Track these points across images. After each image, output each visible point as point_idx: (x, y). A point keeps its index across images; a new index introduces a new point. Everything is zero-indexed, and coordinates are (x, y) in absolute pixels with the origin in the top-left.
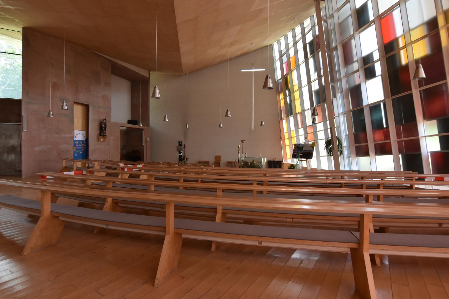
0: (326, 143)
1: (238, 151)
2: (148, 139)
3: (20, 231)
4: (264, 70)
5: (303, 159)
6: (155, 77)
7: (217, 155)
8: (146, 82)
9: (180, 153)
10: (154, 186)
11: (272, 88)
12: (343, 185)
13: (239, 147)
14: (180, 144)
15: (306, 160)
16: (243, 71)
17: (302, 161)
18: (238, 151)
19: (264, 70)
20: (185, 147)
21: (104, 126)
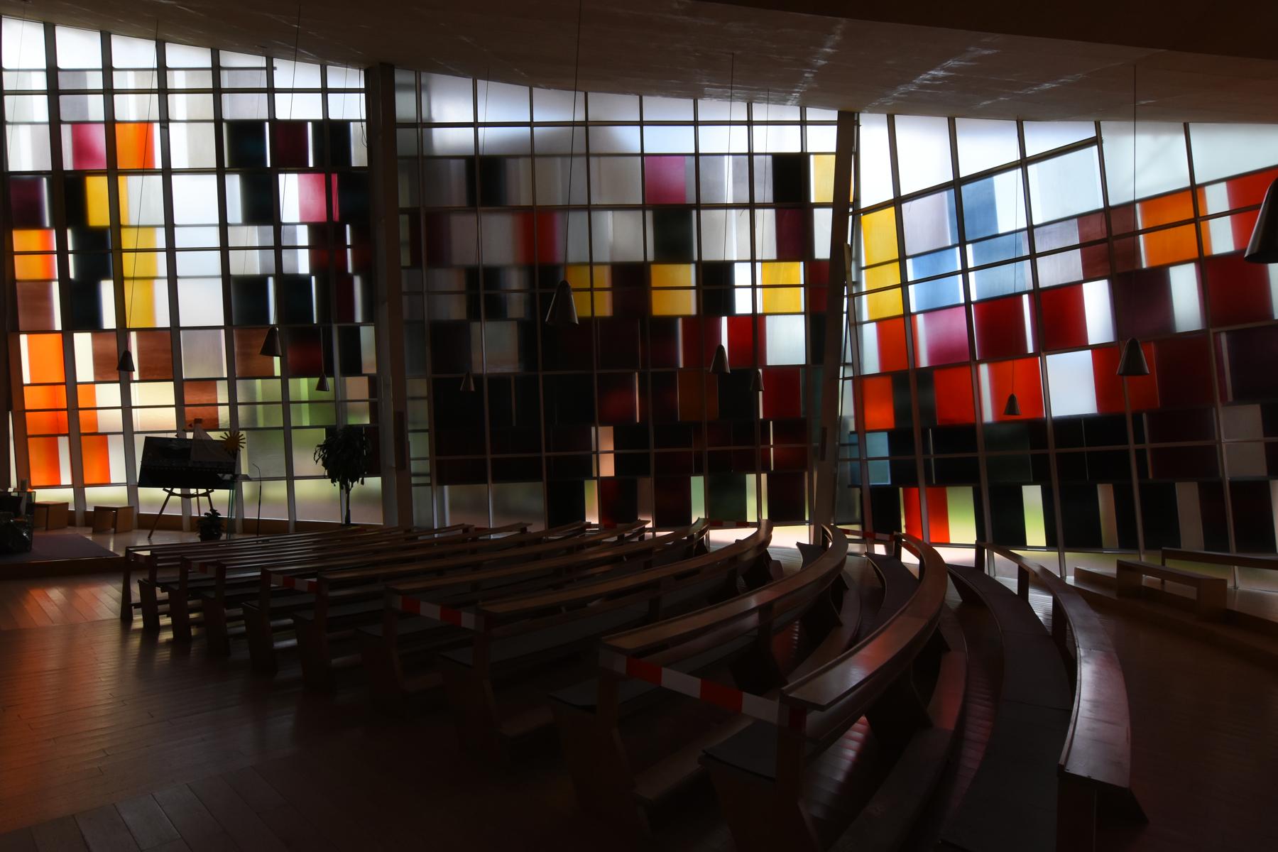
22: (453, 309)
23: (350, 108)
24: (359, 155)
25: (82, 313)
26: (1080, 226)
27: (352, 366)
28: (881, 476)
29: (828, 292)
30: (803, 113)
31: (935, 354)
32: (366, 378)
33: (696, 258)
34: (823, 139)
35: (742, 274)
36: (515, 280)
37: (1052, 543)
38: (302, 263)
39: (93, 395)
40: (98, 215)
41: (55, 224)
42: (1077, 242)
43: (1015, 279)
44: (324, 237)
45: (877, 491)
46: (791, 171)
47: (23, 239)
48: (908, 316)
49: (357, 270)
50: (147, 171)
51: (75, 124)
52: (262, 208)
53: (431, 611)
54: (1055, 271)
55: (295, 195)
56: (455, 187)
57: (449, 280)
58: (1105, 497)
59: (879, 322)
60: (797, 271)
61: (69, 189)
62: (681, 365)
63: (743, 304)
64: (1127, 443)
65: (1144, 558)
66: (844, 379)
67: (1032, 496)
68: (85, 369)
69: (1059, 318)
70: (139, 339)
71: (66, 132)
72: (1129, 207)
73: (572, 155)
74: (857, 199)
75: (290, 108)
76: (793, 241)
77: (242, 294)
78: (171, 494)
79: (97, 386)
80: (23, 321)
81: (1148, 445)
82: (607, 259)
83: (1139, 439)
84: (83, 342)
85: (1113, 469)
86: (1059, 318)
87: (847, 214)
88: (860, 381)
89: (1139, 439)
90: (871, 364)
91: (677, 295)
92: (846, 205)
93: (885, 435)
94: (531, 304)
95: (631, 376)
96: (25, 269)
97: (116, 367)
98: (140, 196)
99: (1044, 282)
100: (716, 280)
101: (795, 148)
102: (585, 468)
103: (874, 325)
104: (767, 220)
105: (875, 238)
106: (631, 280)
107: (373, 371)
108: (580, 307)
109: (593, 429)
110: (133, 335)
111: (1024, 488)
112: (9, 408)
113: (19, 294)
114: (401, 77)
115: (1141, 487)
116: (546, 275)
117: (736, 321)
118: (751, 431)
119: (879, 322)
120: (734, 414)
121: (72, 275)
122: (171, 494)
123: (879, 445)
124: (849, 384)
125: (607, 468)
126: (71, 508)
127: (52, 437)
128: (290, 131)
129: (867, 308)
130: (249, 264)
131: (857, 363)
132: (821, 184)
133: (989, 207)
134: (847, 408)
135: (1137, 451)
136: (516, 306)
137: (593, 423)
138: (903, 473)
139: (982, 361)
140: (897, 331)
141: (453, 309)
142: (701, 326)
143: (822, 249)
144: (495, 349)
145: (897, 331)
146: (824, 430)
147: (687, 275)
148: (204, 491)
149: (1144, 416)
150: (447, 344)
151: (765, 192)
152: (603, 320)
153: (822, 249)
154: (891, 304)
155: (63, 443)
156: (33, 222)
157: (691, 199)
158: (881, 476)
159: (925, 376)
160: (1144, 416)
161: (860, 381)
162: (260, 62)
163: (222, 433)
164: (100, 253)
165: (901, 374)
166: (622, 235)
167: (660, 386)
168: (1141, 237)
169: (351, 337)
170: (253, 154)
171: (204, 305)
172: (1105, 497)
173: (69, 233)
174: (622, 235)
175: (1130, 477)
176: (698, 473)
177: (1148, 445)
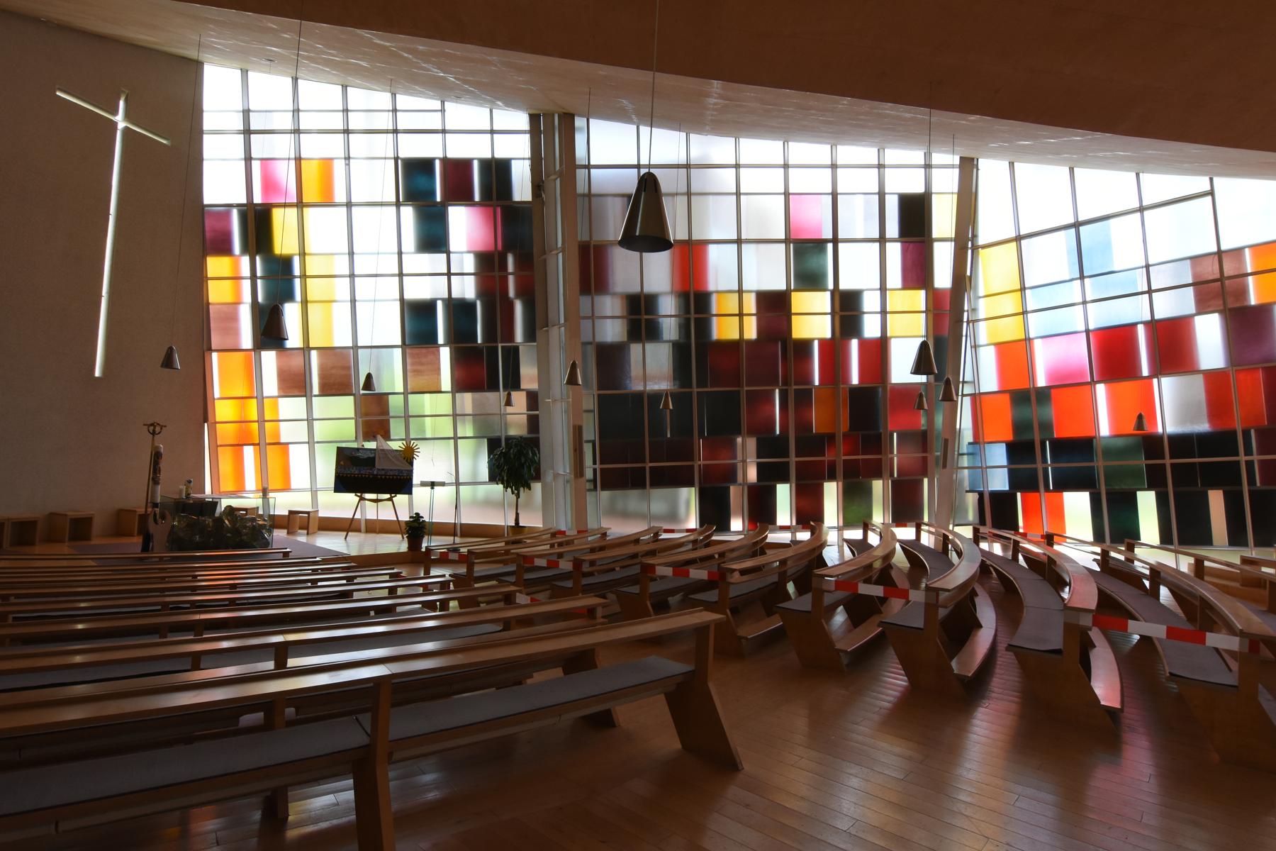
15: (390, 499)
22: (612, 331)
23: (516, 149)
24: (522, 189)
25: (269, 331)
26: (1193, 267)
27: (513, 382)
28: (999, 481)
29: (948, 319)
30: (928, 155)
31: (1051, 375)
32: (524, 393)
33: (831, 286)
34: (945, 185)
35: (870, 302)
36: (668, 306)
37: (1166, 539)
38: (466, 289)
39: (276, 408)
40: (284, 243)
41: (246, 249)
42: (1190, 281)
43: (1133, 312)
44: (488, 264)
45: (996, 496)
46: (915, 213)
47: (216, 265)
48: (1028, 341)
49: (518, 295)
50: (329, 203)
51: (263, 160)
52: (433, 238)
53: (453, 604)
54: (1168, 306)
55: (465, 226)
56: (614, 224)
57: (610, 306)
58: (1216, 501)
59: (999, 346)
60: (918, 298)
61: (258, 223)
62: (817, 383)
63: (871, 328)
64: (1237, 455)
65: (1253, 553)
66: (963, 395)
67: (1147, 502)
68: (271, 385)
69: (1171, 342)
70: (320, 356)
71: (256, 166)
72: (1238, 252)
73: (346, 111)
74: (975, 236)
75: (460, 148)
76: (918, 271)
77: (418, 317)
78: (362, 499)
79: (281, 400)
80: (216, 341)
81: (1256, 457)
82: (755, 288)
83: (1248, 451)
84: (269, 358)
85: (1226, 478)
86: (1171, 342)
87: (967, 248)
88: (976, 398)
89: (1248, 451)
90: (990, 382)
91: (812, 319)
92: (965, 241)
93: (1003, 446)
94: (684, 327)
95: (774, 391)
96: (217, 293)
97: (294, 383)
98: (324, 229)
99: (1159, 315)
100: (847, 308)
101: (919, 189)
102: (730, 475)
103: (992, 348)
104: (895, 251)
105: (993, 270)
106: (775, 306)
107: (534, 386)
108: (724, 330)
109: (739, 440)
110: (314, 354)
111: (1139, 494)
112: (206, 420)
113: (212, 315)
114: (580, 122)
115: (1166, 485)
116: (696, 302)
117: (865, 345)
118: (876, 443)
119: (999, 346)
120: (860, 427)
121: (260, 299)
122: (362, 499)
123: (998, 455)
124: (967, 401)
125: (752, 474)
126: (261, 512)
127: (239, 446)
128: (457, 170)
129: (984, 333)
130: (419, 290)
131: (975, 382)
132: (943, 221)
133: (1106, 247)
134: (965, 421)
135: (1247, 462)
136: (670, 329)
137: (739, 433)
138: (1023, 480)
139: (1099, 382)
140: (1015, 354)
141: (612, 331)
142: (834, 351)
143: (943, 278)
144: (652, 368)
145: (1015, 354)
146: (946, 441)
147: (820, 301)
148: (388, 496)
149: (1253, 432)
150: (610, 360)
151: (893, 229)
152: (749, 342)
153: (943, 278)
154: (1010, 331)
155: (249, 452)
156: (223, 248)
157: (828, 234)
158: (999, 481)
159: (1043, 395)
160: (1253, 432)
161: (976, 398)
162: (436, 104)
163: (400, 443)
164: (280, 278)
165: (1023, 396)
166: (768, 270)
167: (800, 398)
168: (1250, 279)
169: (513, 356)
170: (429, 189)
171: (384, 327)
172: (1216, 501)
173: (258, 258)
174: (768, 270)
175: (1240, 484)
176: (832, 478)
177: (1256, 457)
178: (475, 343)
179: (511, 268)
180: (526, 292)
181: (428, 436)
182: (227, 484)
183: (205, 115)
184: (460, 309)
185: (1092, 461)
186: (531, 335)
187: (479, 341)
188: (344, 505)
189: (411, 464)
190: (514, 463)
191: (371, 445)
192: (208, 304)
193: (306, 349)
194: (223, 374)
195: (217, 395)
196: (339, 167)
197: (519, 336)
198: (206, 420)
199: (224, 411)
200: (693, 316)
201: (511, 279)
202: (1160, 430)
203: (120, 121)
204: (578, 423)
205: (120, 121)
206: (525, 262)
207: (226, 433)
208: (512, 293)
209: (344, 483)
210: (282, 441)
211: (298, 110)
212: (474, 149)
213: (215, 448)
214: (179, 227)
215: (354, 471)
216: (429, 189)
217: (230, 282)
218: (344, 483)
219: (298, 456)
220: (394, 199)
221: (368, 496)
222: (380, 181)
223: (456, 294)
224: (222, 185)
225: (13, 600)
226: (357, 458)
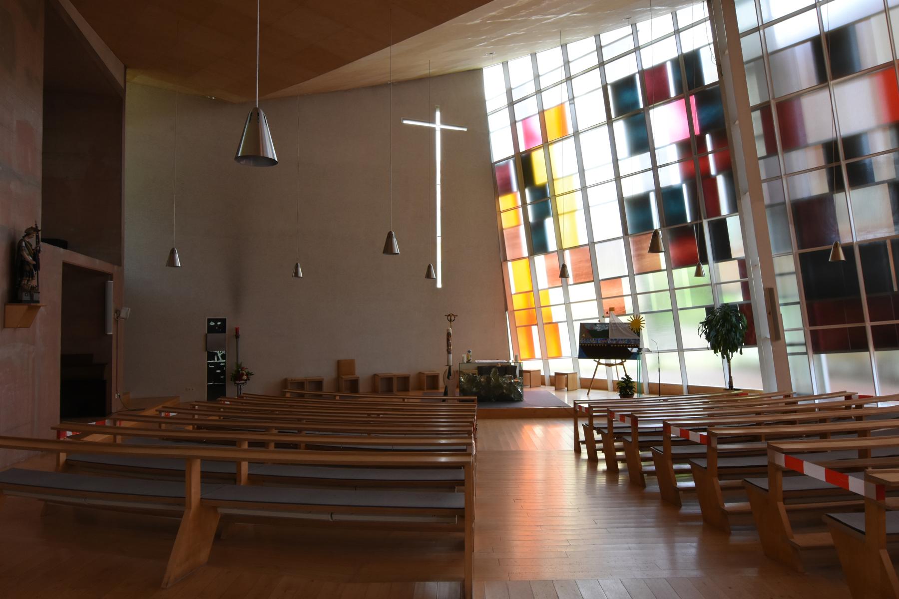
0: (707, 323)
1: (448, 345)
2: (125, 313)
3: (562, 530)
4: (465, 130)
5: (612, 361)
6: (139, 91)
7: (342, 357)
8: (112, 104)
9: (211, 356)
10: (198, 462)
11: (272, 162)
12: (303, 445)
13: (449, 335)
14: (218, 327)
15: (621, 364)
16: (405, 122)
17: (610, 365)
18: (448, 345)
19: (465, 130)
20: (237, 336)
21: (30, 258)
23: (700, 39)
24: (710, 74)
27: (723, 252)
32: (736, 262)
38: (673, 177)
39: (547, 295)
40: (540, 177)
44: (691, 149)
47: (505, 202)
49: (719, 171)
51: (524, 120)
52: (642, 142)
55: (669, 122)
61: (524, 163)
68: (543, 281)
70: (571, 254)
71: (520, 127)
78: (599, 363)
79: (550, 290)
122: (599, 363)
127: (528, 327)
130: (634, 187)
141: (814, 185)
148: (619, 361)
150: (811, 220)
155: (535, 329)
156: (507, 189)
163: (628, 317)
164: (543, 200)
169: (720, 230)
173: (527, 191)
178: (676, 228)
179: (709, 148)
180: (726, 167)
181: (655, 309)
182: (524, 354)
183: (487, 103)
184: (669, 196)
185: (398, 391)
186: (734, 208)
187: (689, 220)
188: (588, 368)
189: (638, 334)
190: (727, 329)
191: (607, 320)
192: (502, 229)
193: (561, 251)
194: (516, 274)
195: (513, 291)
196: (567, 106)
197: (724, 209)
198: (506, 310)
199: (518, 302)
200: (843, 163)
201: (711, 157)
202: (512, 361)
203: (438, 126)
204: (770, 286)
205: (438, 126)
206: (722, 140)
207: (521, 318)
208: (713, 171)
209: (586, 351)
210: (554, 321)
211: (569, 62)
212: (661, 54)
213: (515, 328)
214: (481, 179)
215: (593, 341)
216: (630, 102)
217: (512, 211)
218: (586, 351)
219: (563, 329)
220: (604, 119)
221: (603, 361)
222: (592, 107)
223: (663, 184)
224: (501, 148)
225: (275, 431)
226: (595, 331)
